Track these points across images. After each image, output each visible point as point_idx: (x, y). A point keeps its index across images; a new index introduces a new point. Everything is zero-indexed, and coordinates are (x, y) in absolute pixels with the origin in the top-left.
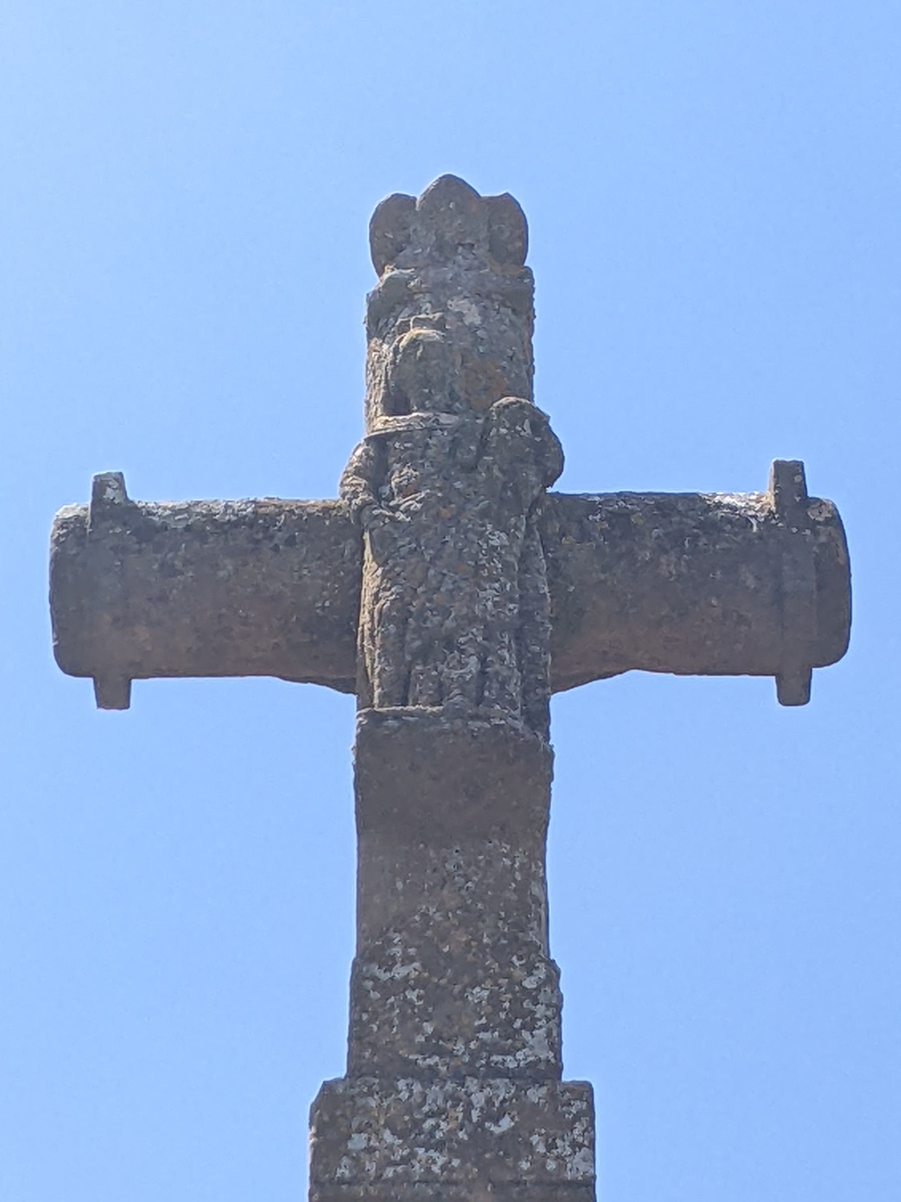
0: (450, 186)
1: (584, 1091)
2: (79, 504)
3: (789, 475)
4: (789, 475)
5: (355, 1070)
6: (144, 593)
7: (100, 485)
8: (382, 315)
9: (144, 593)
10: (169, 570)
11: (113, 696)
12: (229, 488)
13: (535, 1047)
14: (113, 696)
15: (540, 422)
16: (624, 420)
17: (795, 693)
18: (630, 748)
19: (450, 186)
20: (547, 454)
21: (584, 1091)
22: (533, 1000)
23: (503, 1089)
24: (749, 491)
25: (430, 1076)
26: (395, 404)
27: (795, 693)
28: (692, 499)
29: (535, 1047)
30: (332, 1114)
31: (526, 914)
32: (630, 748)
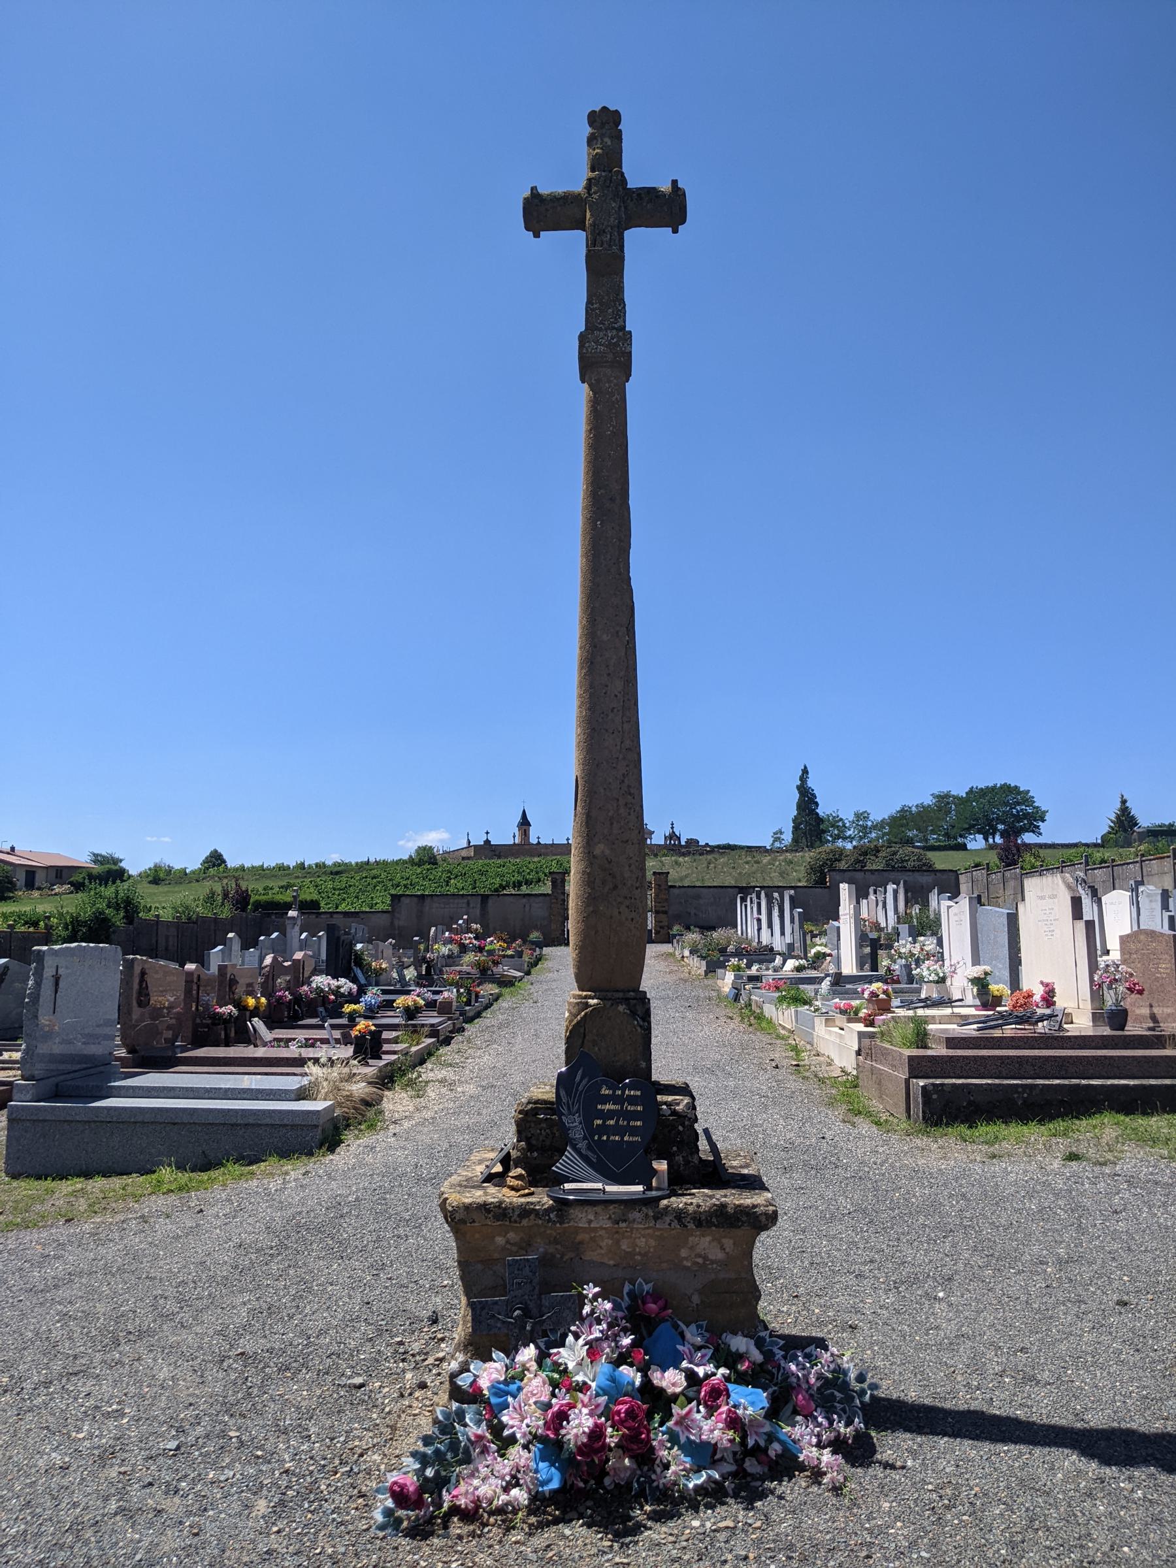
0: (605, 109)
1: (630, 332)
2: (527, 193)
3: (675, 182)
4: (675, 182)
5: (587, 329)
6: (542, 213)
7: (532, 189)
8: (591, 140)
9: (542, 213)
10: (547, 210)
11: (537, 235)
12: (560, 189)
13: (621, 323)
14: (537, 235)
15: (622, 174)
16: (640, 170)
17: (675, 231)
18: (640, 243)
19: (605, 109)
20: (624, 181)
21: (630, 332)
22: (620, 313)
23: (614, 332)
24: (665, 187)
25: (600, 330)
26: (593, 170)
27: (675, 231)
28: (654, 188)
29: (621, 323)
30: (582, 338)
31: (621, 289)
32: (640, 243)
